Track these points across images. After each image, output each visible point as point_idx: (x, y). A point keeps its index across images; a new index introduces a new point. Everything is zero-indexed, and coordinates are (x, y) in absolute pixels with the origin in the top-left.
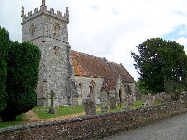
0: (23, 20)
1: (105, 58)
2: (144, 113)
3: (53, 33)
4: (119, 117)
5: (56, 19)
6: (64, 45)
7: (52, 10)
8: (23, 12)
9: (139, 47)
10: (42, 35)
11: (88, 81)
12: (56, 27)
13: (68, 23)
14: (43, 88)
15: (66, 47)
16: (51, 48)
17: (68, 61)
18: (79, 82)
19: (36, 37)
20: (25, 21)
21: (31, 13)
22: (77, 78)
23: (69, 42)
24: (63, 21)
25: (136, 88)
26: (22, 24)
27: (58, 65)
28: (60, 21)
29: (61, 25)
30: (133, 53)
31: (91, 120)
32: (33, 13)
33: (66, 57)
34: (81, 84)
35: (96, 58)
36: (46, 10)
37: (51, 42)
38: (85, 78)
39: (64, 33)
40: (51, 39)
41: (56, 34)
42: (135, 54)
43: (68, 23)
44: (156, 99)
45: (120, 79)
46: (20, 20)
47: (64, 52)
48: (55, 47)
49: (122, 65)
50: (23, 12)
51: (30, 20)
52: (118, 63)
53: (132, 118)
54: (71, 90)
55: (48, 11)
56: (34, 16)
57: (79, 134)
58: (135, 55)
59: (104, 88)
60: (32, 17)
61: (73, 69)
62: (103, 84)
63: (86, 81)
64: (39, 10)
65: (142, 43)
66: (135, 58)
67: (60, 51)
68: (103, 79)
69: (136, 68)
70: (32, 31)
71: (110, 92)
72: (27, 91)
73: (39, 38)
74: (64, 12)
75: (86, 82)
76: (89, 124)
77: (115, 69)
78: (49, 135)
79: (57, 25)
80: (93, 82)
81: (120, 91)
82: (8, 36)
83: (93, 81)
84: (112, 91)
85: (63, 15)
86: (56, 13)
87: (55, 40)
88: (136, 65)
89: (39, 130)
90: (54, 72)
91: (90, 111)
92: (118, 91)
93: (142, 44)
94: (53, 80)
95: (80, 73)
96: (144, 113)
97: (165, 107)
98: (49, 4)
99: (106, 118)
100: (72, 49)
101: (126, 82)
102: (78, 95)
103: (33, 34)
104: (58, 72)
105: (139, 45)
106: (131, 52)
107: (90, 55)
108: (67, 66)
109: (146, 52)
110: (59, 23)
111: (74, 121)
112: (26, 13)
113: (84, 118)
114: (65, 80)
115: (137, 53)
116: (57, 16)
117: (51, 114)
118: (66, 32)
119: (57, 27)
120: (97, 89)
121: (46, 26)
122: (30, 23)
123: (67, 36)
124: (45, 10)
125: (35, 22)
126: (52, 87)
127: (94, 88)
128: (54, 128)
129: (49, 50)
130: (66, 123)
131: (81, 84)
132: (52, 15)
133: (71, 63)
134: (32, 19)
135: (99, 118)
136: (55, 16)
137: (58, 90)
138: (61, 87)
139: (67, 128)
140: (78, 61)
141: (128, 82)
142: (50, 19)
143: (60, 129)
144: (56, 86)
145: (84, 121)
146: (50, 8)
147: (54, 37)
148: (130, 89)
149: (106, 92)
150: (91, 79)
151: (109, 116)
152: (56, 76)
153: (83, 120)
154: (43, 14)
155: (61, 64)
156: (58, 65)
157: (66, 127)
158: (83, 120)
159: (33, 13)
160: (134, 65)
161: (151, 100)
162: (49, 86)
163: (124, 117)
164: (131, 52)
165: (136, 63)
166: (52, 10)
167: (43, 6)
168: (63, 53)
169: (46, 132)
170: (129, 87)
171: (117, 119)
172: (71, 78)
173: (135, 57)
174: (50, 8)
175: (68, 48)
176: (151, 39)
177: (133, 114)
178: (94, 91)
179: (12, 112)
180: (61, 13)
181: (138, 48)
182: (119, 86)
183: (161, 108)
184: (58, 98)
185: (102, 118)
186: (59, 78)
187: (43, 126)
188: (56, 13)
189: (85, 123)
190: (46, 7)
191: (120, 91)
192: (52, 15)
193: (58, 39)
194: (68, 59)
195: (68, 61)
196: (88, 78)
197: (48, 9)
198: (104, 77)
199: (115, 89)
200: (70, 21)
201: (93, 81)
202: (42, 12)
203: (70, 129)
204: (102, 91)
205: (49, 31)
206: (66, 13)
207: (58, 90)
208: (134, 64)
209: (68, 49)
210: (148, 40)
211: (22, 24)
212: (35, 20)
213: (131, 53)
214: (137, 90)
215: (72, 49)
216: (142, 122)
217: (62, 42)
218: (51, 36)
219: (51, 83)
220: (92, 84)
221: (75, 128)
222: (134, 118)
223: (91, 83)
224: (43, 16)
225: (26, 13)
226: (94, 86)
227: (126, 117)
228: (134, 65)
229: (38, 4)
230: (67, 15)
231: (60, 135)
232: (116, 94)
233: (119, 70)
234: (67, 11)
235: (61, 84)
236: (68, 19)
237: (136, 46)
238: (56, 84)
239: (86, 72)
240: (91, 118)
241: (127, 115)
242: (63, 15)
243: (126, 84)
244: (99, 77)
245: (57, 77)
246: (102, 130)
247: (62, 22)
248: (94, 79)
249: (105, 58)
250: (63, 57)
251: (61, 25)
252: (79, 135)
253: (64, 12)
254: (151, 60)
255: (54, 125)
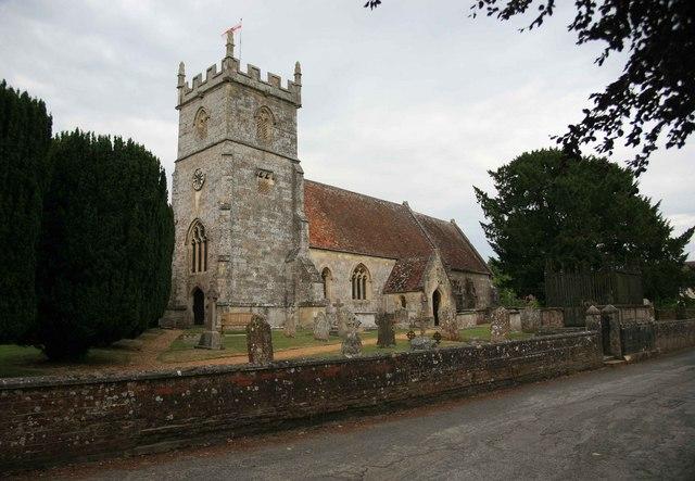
1: (405, 204)
3: (254, 131)
5: (265, 94)
7: (255, 71)
8: (181, 76)
9: (498, 175)
10: (222, 138)
11: (350, 265)
12: (264, 116)
13: (300, 106)
15: (289, 171)
16: (246, 172)
17: (294, 208)
18: (320, 269)
19: (209, 143)
20: (186, 99)
22: (316, 257)
23: (299, 157)
24: (284, 100)
26: (177, 108)
30: (481, 193)
33: (288, 199)
36: (238, 69)
37: (247, 158)
38: (340, 255)
40: (249, 150)
41: (262, 135)
43: (300, 106)
44: (523, 325)
45: (437, 263)
46: (174, 97)
47: (283, 184)
49: (455, 225)
50: (181, 76)
51: (196, 97)
52: (140, 144)
53: (384, 379)
54: (300, 283)
55: (242, 74)
56: (206, 87)
57: (171, 417)
58: (488, 200)
59: (394, 285)
60: (202, 89)
61: (306, 230)
62: (393, 273)
63: (343, 265)
64: (219, 70)
65: (507, 163)
67: (271, 182)
70: (200, 126)
71: (408, 296)
74: (286, 77)
76: (214, 391)
78: (59, 415)
80: (361, 268)
81: (437, 296)
82: (48, 122)
83: (361, 265)
84: (415, 294)
85: (284, 85)
87: (259, 153)
88: (490, 227)
89: (20, 399)
90: (251, 235)
91: (259, 350)
92: (430, 296)
93: (508, 168)
98: (246, 59)
100: (306, 177)
103: (202, 134)
106: (477, 189)
108: (289, 223)
109: (519, 192)
110: (273, 107)
112: (189, 80)
114: (283, 260)
115: (493, 194)
117: (205, 352)
118: (293, 131)
120: (373, 289)
122: (197, 104)
123: (295, 141)
125: (210, 102)
126: (244, 276)
127: (364, 284)
128: (79, 394)
129: (241, 178)
130: (127, 381)
134: (201, 96)
136: (262, 87)
138: (271, 278)
139: (128, 396)
140: (324, 208)
143: (102, 399)
144: (255, 274)
145: (194, 381)
149: (397, 297)
150: (356, 260)
151: (293, 371)
152: (258, 247)
153: (190, 377)
154: (227, 80)
156: (264, 219)
157: (125, 394)
158: (190, 377)
161: (516, 323)
162: (235, 272)
164: (477, 189)
166: (254, 72)
167: (230, 61)
169: (46, 405)
170: (469, 286)
172: (300, 254)
178: (364, 293)
179: (69, 338)
180: (279, 79)
182: (436, 279)
183: (501, 354)
185: (266, 376)
186: (265, 253)
187: (38, 389)
189: (197, 387)
190: (236, 62)
191: (437, 296)
192: (251, 83)
193: (270, 149)
194: (294, 204)
195: (294, 208)
196: (347, 257)
197: (244, 69)
199: (422, 289)
200: (303, 102)
201: (361, 265)
202: (225, 75)
203: (137, 403)
204: (389, 292)
205: (242, 129)
207: (262, 286)
209: (294, 176)
210: (525, 155)
211: (177, 108)
212: (208, 97)
213: (474, 194)
214: (492, 296)
215: (306, 177)
216: (424, 393)
217: (278, 158)
218: (247, 140)
219: (244, 266)
220: (359, 273)
221: (158, 398)
223: (356, 271)
224: (228, 86)
226: (364, 280)
227: (361, 374)
229: (217, 59)
230: (296, 86)
231: (99, 419)
232: (424, 302)
233: (448, 238)
234: (298, 75)
235: (272, 270)
236: (298, 98)
242: (284, 85)
243: (461, 278)
244: (382, 254)
246: (260, 412)
247: (282, 104)
248: (365, 260)
249: (405, 204)
250: (280, 197)
251: (281, 114)
252: (170, 422)
253: (286, 77)
255: (82, 386)
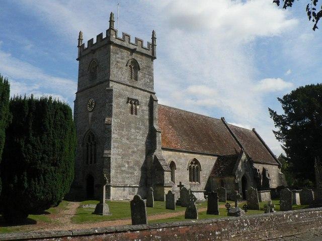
0: (80, 54)
2: (244, 227)
4: (185, 232)
5: (133, 51)
6: (146, 97)
8: (80, 39)
13: (155, 58)
14: (103, 168)
16: (122, 101)
18: (168, 162)
20: (83, 54)
21: (93, 42)
25: (279, 174)
26: (77, 60)
27: (133, 130)
28: (143, 57)
29: (142, 62)
30: (272, 111)
31: (119, 235)
32: (95, 41)
34: (172, 165)
35: (206, 119)
38: (181, 153)
39: (147, 76)
42: (276, 112)
48: (129, 99)
50: (80, 39)
52: (249, 128)
53: (214, 234)
56: (96, 47)
63: (183, 160)
66: (276, 120)
68: (216, 158)
69: (278, 138)
72: (44, 175)
73: (102, 83)
75: (182, 161)
77: (242, 139)
79: (134, 62)
80: (196, 161)
83: (195, 160)
85: (145, 45)
86: (133, 41)
88: (279, 133)
90: (124, 141)
94: (123, 156)
95: (173, 145)
96: (244, 227)
97: (299, 217)
99: (155, 232)
101: (260, 163)
102: (166, 182)
104: (133, 142)
105: (285, 97)
107: (196, 114)
111: (84, 234)
113: (105, 231)
115: (281, 112)
116: (135, 47)
119: (135, 67)
121: (115, 63)
123: (152, 80)
124: (114, 36)
131: (172, 165)
132: (126, 46)
133: (156, 127)
134: (93, 51)
135: (138, 232)
136: (132, 47)
137: (131, 173)
140: (171, 123)
141: (263, 164)
142: (122, 52)
144: (127, 166)
146: (123, 33)
147: (128, 83)
148: (267, 176)
150: (191, 157)
151: (161, 230)
152: (129, 148)
153: (102, 234)
155: (140, 129)
156: (133, 130)
159: (95, 41)
160: (274, 132)
163: (194, 233)
164: (270, 110)
165: (278, 129)
168: (143, 111)
171: (178, 236)
173: (277, 119)
174: (123, 33)
175: (152, 102)
176: (307, 87)
177: (217, 228)
181: (283, 102)
184: (129, 187)
185: (145, 232)
186: (133, 152)
188: (133, 41)
192: (125, 44)
193: (135, 85)
198: (217, 153)
206: (151, 42)
207: (131, 173)
208: (273, 131)
210: (312, 86)
211: (77, 60)
212: (97, 53)
213: (269, 112)
215: (161, 102)
217: (142, 92)
218: (122, 80)
219: (120, 161)
222: (219, 235)
223: (192, 163)
225: (85, 42)
227: (200, 232)
228: (274, 132)
234: (154, 38)
237: (279, 99)
238: (128, 163)
239: (185, 144)
240: (120, 232)
241: (203, 230)
242: (145, 45)
245: (130, 151)
248: (197, 157)
253: (147, 40)
254: (307, 125)
